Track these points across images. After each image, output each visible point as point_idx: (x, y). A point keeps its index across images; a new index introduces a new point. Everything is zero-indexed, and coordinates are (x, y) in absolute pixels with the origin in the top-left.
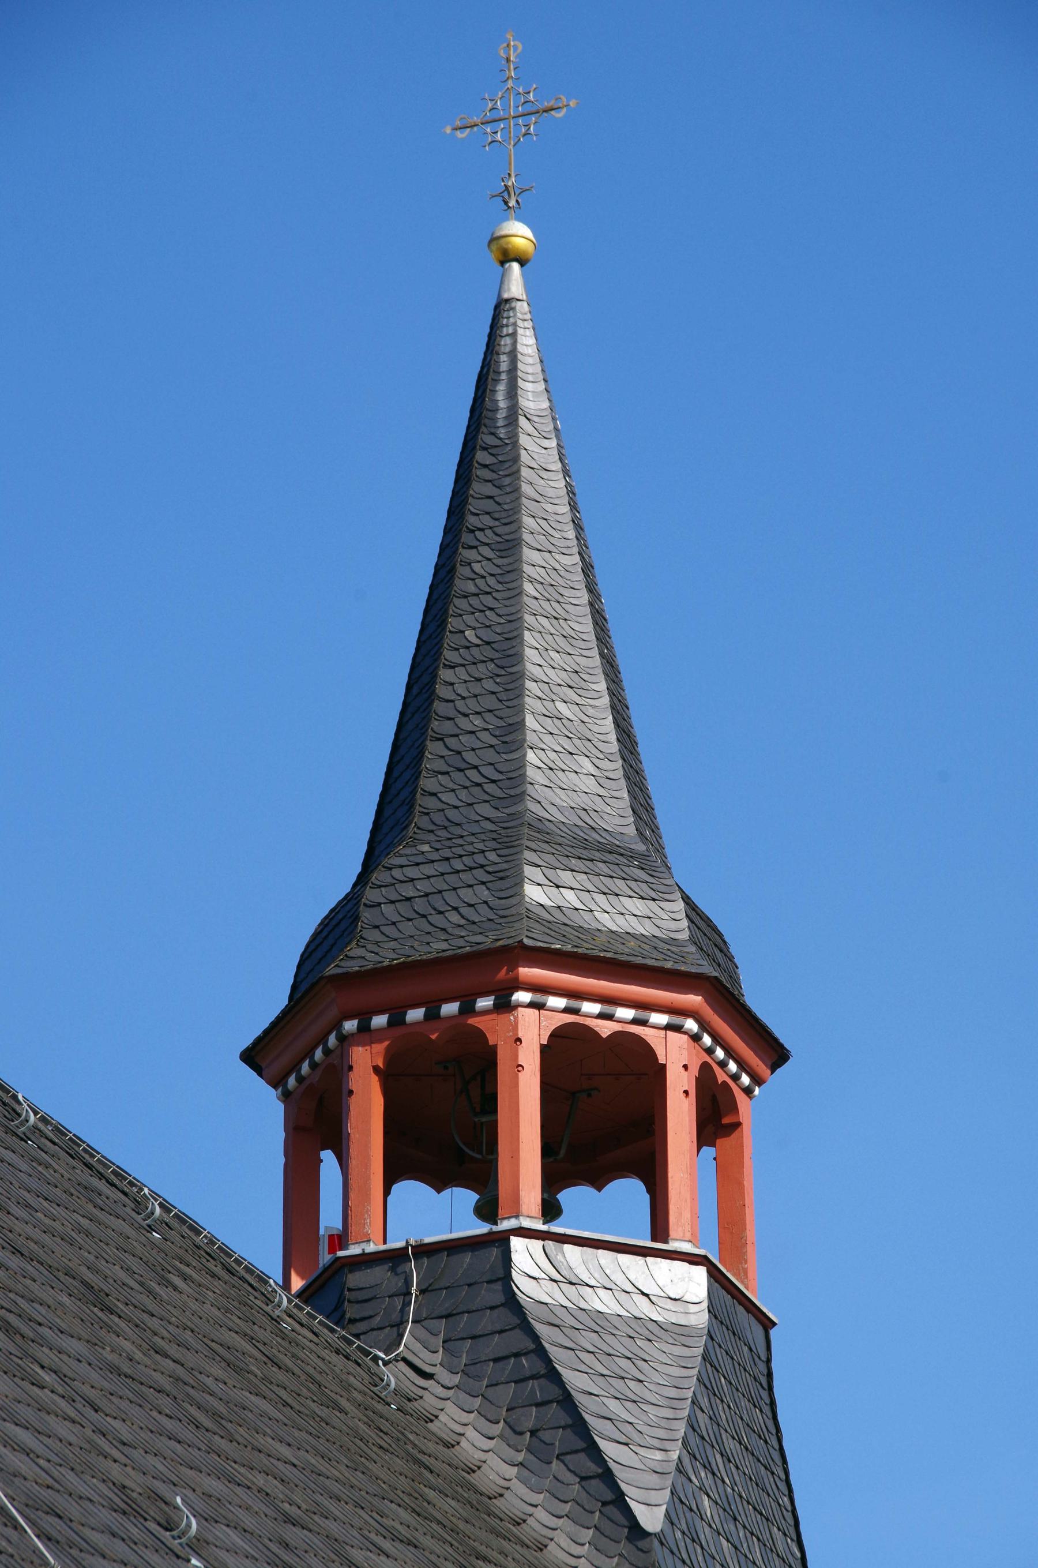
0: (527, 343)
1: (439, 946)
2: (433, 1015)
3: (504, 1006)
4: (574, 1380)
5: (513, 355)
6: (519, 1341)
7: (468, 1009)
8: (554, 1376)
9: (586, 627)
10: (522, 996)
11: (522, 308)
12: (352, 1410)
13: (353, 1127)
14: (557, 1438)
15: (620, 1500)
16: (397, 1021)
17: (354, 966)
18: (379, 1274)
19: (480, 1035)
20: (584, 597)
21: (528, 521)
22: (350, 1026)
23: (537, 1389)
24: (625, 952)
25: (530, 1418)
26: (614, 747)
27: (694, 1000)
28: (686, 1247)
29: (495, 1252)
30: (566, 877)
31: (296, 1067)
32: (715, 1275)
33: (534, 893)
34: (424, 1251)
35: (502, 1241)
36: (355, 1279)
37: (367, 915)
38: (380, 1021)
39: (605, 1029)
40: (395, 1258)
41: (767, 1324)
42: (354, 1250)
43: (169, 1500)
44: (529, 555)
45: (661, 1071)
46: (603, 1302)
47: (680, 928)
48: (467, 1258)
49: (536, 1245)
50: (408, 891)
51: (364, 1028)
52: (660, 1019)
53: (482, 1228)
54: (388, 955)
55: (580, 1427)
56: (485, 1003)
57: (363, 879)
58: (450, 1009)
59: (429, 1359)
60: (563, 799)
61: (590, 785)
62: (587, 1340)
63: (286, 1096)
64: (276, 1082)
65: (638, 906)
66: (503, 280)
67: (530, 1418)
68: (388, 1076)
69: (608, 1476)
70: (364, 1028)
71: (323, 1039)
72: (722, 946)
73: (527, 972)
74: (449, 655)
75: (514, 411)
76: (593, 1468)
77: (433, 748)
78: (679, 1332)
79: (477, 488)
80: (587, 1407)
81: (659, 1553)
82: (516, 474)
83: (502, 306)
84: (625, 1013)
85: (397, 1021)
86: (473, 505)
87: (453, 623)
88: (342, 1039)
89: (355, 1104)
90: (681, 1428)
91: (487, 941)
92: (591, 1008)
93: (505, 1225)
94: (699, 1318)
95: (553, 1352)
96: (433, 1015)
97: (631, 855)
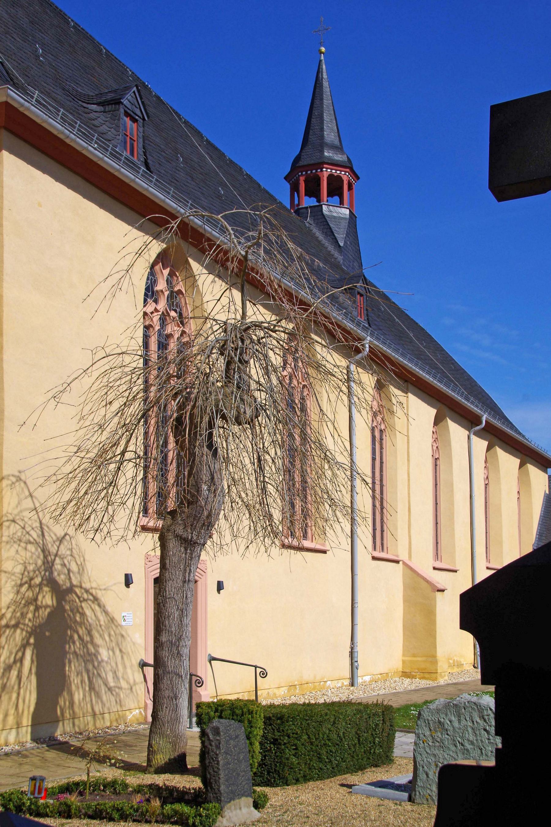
0: (324, 67)
1: (312, 162)
2: (311, 172)
3: (322, 171)
4: (331, 225)
5: (322, 69)
6: (324, 220)
7: (316, 171)
8: (328, 224)
9: (333, 112)
10: (324, 169)
11: (323, 61)
12: (223, 230)
13: (300, 189)
14: (329, 233)
15: (337, 242)
16: (306, 173)
17: (300, 165)
18: (304, 210)
19: (318, 175)
20: (332, 108)
21: (324, 96)
22: (300, 174)
23: (326, 227)
24: (339, 163)
25: (325, 230)
26: (336, 131)
27: (348, 170)
28: (346, 206)
29: (320, 207)
30: (330, 151)
31: (292, 180)
32: (350, 211)
33: (326, 154)
34: (310, 207)
35: (321, 205)
36: (301, 211)
37: (302, 157)
38: (304, 173)
39: (336, 174)
40: (306, 208)
41: (356, 217)
42: (301, 207)
43: (397, 704)
44: (324, 101)
45: (343, 181)
46: (335, 214)
47: (346, 159)
48: (316, 208)
49: (326, 206)
50: (308, 153)
51: (302, 174)
52: (343, 173)
53: (318, 204)
54: (305, 163)
55: (332, 232)
56: (319, 170)
57: (301, 151)
58: (314, 171)
59: (312, 222)
60: (330, 139)
61: (333, 137)
62: (333, 220)
63: (290, 184)
64: (288, 182)
65: (340, 156)
66: (320, 57)
67: (325, 230)
68: (305, 181)
69: (336, 239)
70: (302, 174)
71: (296, 176)
72: (351, 162)
73: (325, 166)
74: (313, 117)
75: (322, 77)
76: (333, 237)
77: (311, 131)
78: (345, 219)
79: (317, 90)
80: (333, 229)
81: (343, 249)
82: (322, 88)
83: (320, 61)
84: (338, 172)
85: (306, 173)
86: (316, 93)
87: (314, 112)
88: (299, 176)
89: (300, 185)
90: (345, 232)
91: (320, 161)
92: (334, 171)
93: (322, 203)
94: (348, 217)
95: (329, 222)
96: (311, 172)
97: (339, 148)
